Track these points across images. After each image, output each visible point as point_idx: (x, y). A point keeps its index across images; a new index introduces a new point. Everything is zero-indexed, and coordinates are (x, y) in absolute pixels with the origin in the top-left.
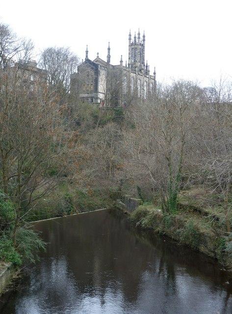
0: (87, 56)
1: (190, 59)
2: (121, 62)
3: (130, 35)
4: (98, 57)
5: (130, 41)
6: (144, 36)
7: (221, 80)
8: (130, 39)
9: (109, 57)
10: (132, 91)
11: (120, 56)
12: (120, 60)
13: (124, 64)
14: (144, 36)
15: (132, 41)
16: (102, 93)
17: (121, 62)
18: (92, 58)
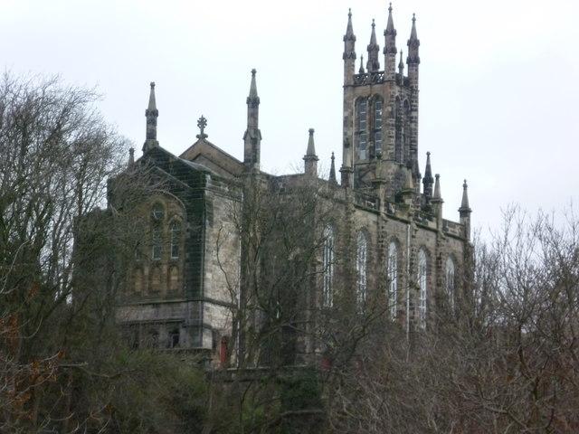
14: (413, 44)
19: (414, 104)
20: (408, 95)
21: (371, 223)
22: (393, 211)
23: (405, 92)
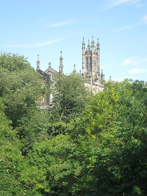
14: (98, 45)
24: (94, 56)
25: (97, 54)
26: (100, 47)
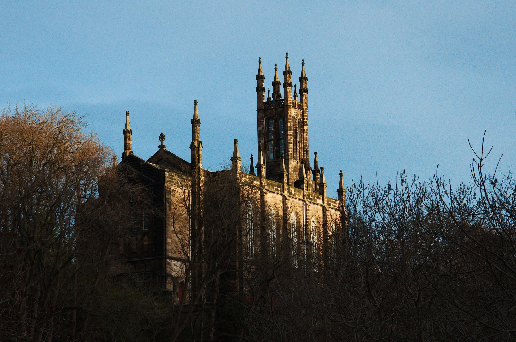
0: (126, 147)
1: (409, 130)
2: (235, 159)
3: (260, 78)
4: (162, 147)
5: (260, 97)
6: (303, 79)
7: (276, 69)
8: (260, 90)
9: (195, 148)
10: (273, 248)
11: (230, 138)
12: (231, 155)
13: (243, 164)
14: (303, 79)
15: (266, 94)
16: (177, 259)
17: (235, 159)
18: (144, 150)
19: (305, 120)
20: (300, 114)
21: (278, 202)
22: (293, 193)
23: (299, 112)
24: (292, 112)
25: (301, 107)
26: (309, 85)
